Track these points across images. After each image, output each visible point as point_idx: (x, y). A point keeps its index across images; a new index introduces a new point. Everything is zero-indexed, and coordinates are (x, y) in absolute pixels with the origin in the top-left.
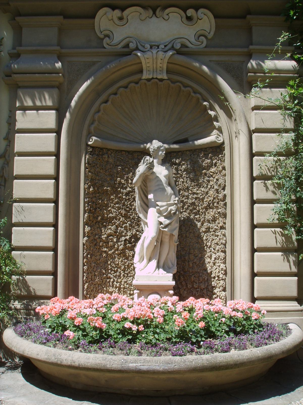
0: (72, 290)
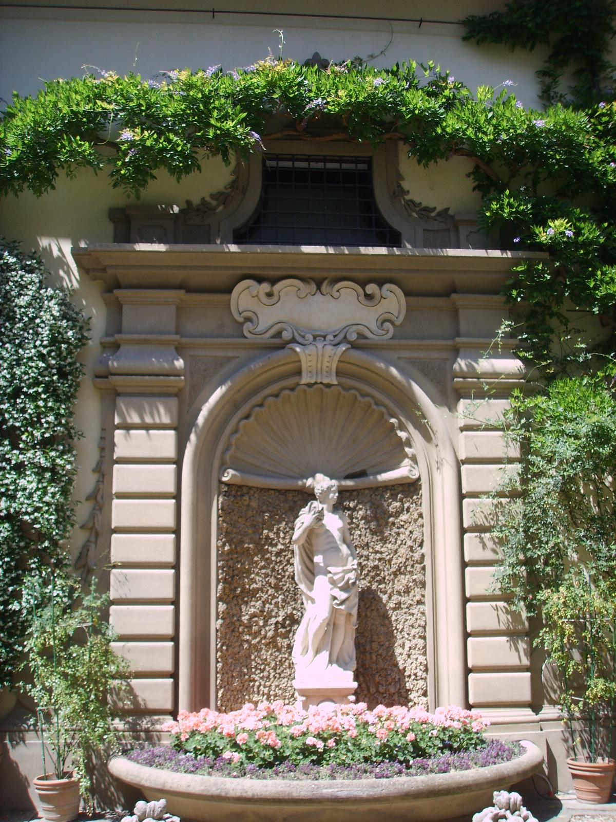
0: (200, 701)
